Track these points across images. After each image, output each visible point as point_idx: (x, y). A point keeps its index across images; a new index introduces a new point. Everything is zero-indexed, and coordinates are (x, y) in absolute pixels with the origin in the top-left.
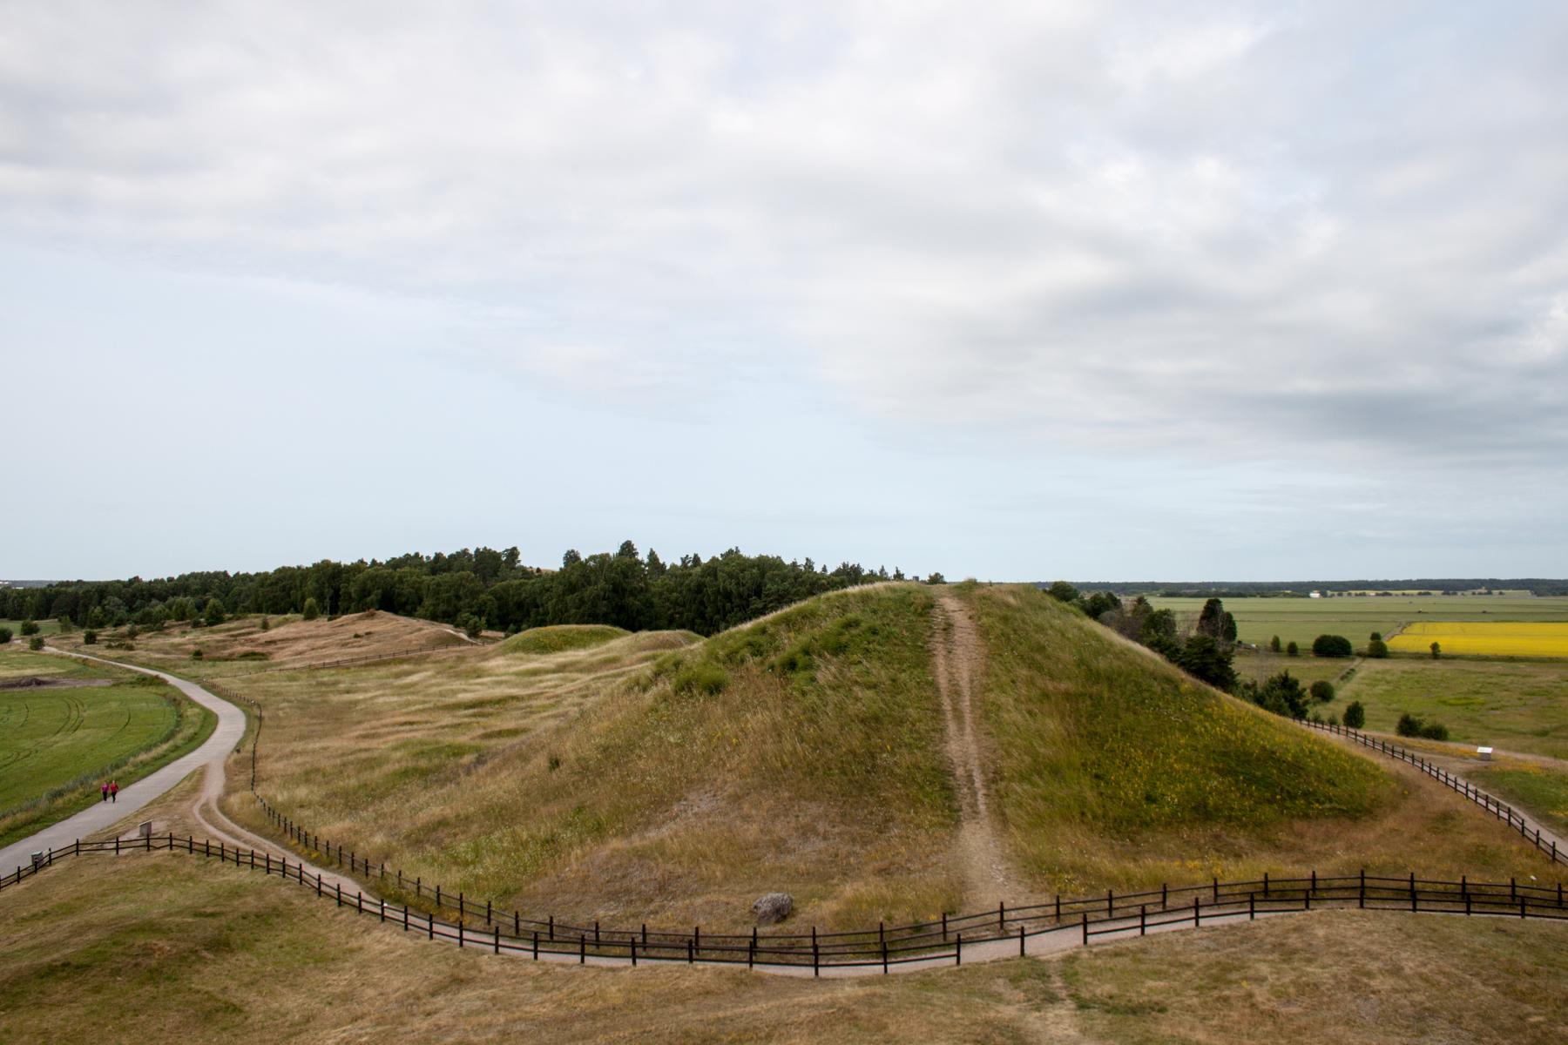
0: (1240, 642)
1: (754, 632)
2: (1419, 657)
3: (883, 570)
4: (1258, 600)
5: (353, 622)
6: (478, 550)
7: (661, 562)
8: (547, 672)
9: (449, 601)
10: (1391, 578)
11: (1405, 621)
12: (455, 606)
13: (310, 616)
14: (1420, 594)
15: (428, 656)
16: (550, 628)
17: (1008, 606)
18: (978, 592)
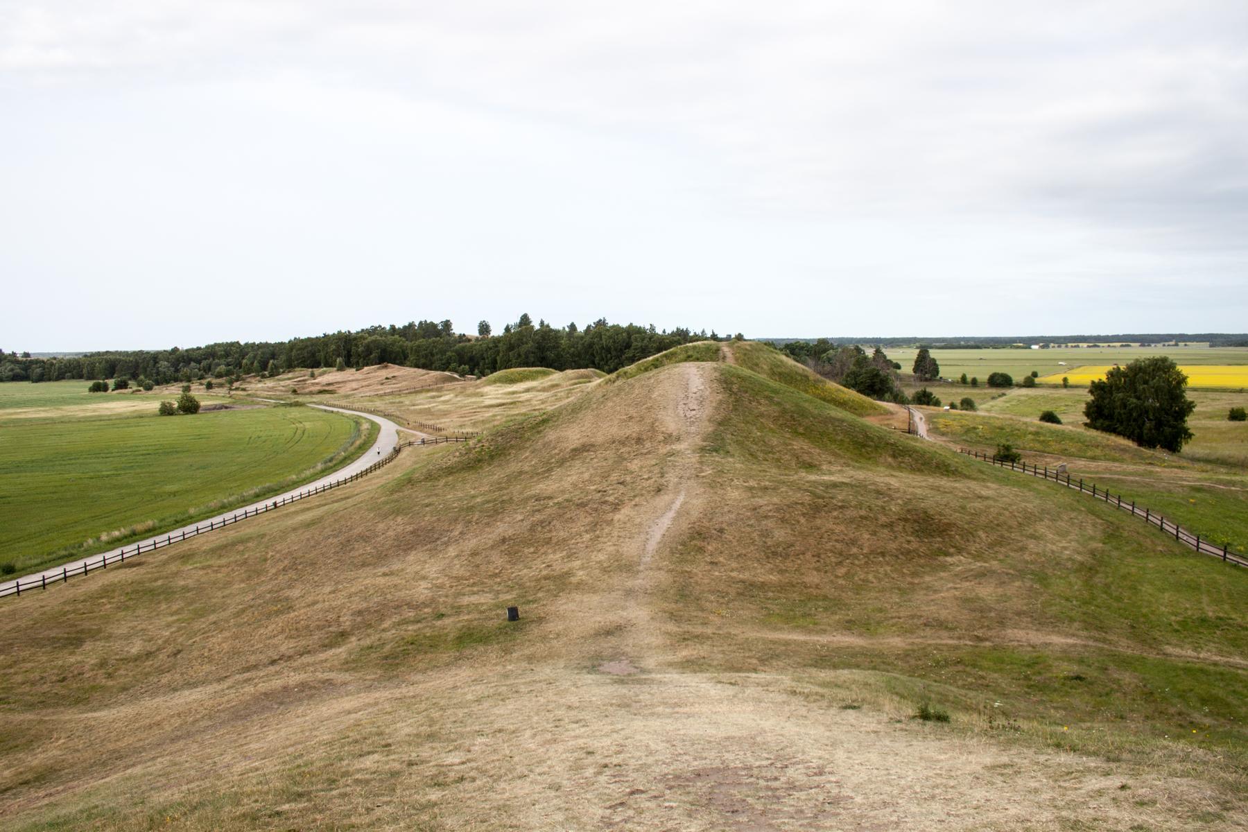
0: (941, 378)
1: (653, 360)
2: (1055, 386)
3: (703, 331)
4: (990, 351)
5: (375, 371)
6: (421, 323)
8: (520, 393)
9: (426, 356)
10: (1103, 333)
11: (1053, 364)
12: (430, 360)
13: (341, 369)
14: (1122, 346)
15: (442, 387)
16: (512, 369)
17: (746, 349)
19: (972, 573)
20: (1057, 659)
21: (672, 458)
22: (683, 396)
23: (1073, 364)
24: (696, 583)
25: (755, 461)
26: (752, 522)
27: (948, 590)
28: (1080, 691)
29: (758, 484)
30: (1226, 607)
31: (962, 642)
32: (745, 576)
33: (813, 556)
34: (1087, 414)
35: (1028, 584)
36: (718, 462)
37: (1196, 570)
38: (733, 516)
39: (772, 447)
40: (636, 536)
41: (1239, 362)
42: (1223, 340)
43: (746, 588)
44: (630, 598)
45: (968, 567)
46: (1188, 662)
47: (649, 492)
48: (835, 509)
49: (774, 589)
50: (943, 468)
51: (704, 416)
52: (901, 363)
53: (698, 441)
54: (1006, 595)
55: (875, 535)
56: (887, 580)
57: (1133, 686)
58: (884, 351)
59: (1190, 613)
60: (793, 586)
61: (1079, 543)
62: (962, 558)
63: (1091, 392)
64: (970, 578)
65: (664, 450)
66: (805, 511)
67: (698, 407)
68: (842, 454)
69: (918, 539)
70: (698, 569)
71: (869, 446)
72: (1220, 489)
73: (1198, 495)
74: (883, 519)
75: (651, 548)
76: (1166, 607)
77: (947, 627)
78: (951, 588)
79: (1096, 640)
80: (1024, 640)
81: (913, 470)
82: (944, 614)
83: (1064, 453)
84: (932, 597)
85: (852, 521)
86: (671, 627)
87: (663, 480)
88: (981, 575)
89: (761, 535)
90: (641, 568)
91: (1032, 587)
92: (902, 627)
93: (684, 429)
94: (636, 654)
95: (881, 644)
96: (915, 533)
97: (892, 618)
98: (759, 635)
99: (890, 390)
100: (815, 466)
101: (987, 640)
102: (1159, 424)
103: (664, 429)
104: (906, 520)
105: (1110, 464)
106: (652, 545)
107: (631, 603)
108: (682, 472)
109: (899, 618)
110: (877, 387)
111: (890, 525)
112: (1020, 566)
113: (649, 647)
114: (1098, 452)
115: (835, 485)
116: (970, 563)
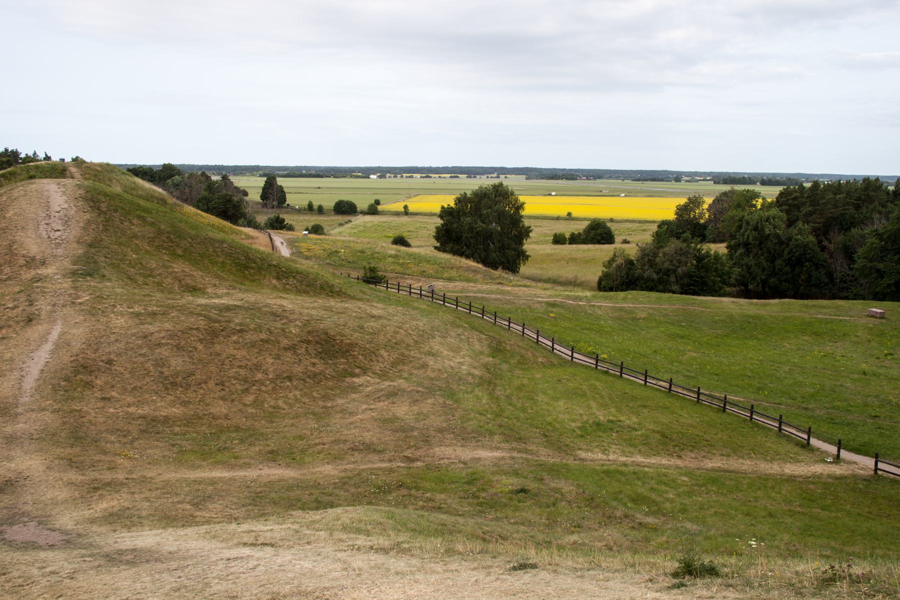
0: (288, 205)
2: (397, 214)
3: (35, 154)
4: (331, 179)
7: (58, 160)
10: (434, 164)
11: (396, 192)
17: (97, 170)
18: (85, 165)
19: (383, 392)
20: (493, 473)
21: (39, 284)
22: (44, 215)
23: (412, 193)
24: (90, 422)
25: (135, 285)
26: (144, 351)
27: (364, 411)
28: (528, 504)
29: (145, 309)
30: (613, 410)
31: (394, 465)
32: (145, 410)
33: (217, 384)
34: (437, 238)
35: (441, 400)
36: (95, 287)
37: (577, 378)
38: (122, 345)
39: (152, 270)
40: (8, 374)
41: (578, 193)
42: (537, 174)
43: (148, 424)
44: (14, 446)
45: (377, 387)
46: (603, 465)
47: (18, 322)
48: (234, 334)
49: (179, 423)
50: (328, 290)
51: (71, 237)
52: (248, 190)
53: (67, 264)
54: (422, 413)
55: (279, 359)
56: (298, 405)
57: (574, 493)
58: (232, 178)
59: (585, 418)
60: (200, 418)
61: (472, 358)
62: (368, 378)
63: (441, 216)
64: (383, 398)
65: (27, 275)
66: (202, 337)
67: (63, 228)
68: (225, 276)
69: (323, 362)
70: (90, 406)
71: (253, 268)
72: (570, 304)
73: (555, 310)
74: (285, 342)
75: (28, 387)
76: (564, 414)
77: (375, 451)
78: (366, 409)
79: (519, 451)
80: (453, 457)
81: (299, 292)
82: (368, 437)
83: (423, 274)
84: (350, 420)
85: (253, 345)
86: (73, 475)
87: (33, 309)
88: (392, 394)
89: (156, 365)
90: (20, 410)
91: (445, 403)
92: (330, 454)
93: (48, 251)
94: (40, 512)
95: (313, 473)
96: (318, 354)
97: (316, 444)
98: (178, 476)
99: (243, 215)
100: (200, 289)
101: (417, 460)
102: (503, 248)
103: (25, 252)
104: (308, 342)
105: (465, 284)
106: (29, 383)
107: (17, 452)
108: (55, 299)
109: (324, 444)
110: (230, 213)
111: (292, 348)
112: (427, 383)
113: (55, 503)
114: (454, 273)
115: (228, 308)
116: (378, 383)
